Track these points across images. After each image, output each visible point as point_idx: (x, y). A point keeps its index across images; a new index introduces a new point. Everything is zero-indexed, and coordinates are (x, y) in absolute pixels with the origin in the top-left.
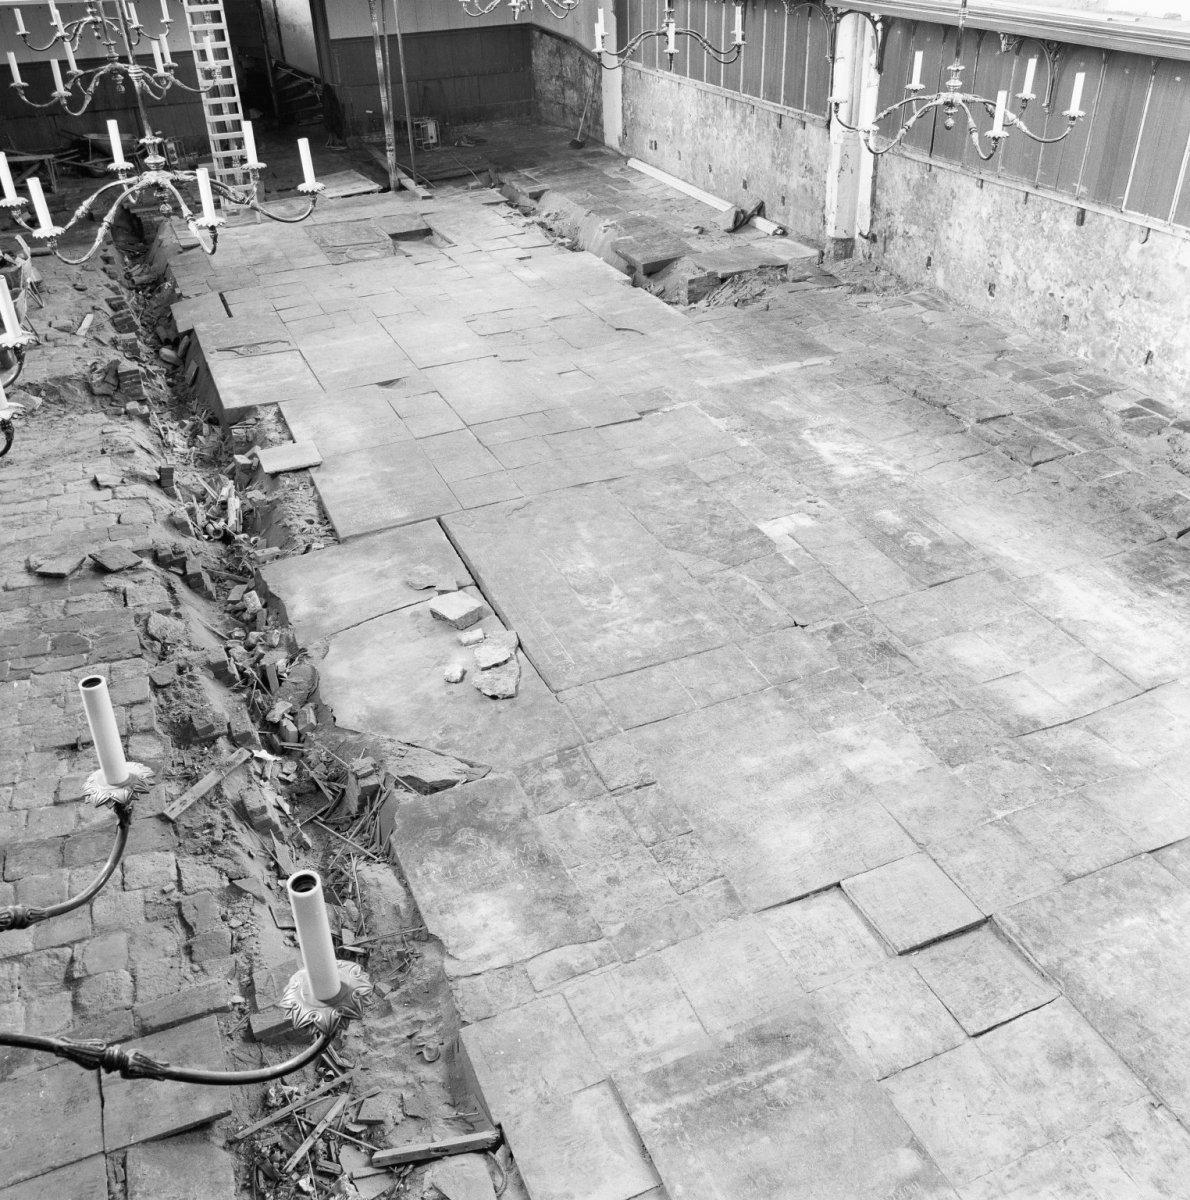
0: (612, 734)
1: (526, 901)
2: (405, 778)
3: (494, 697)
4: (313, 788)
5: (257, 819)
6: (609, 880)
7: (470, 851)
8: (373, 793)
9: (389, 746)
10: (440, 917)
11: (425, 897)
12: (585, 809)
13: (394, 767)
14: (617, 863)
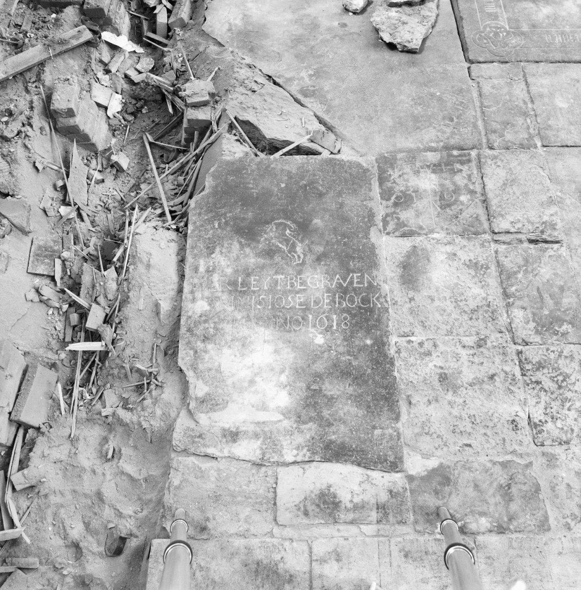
0: (525, 146)
1: (320, 367)
2: (246, 124)
3: (392, 46)
4: (158, 97)
5: (63, 122)
6: (443, 378)
7: (277, 258)
8: (205, 128)
9: (244, 73)
10: (200, 345)
11: (196, 307)
12: (449, 249)
13: (235, 106)
14: (464, 353)
